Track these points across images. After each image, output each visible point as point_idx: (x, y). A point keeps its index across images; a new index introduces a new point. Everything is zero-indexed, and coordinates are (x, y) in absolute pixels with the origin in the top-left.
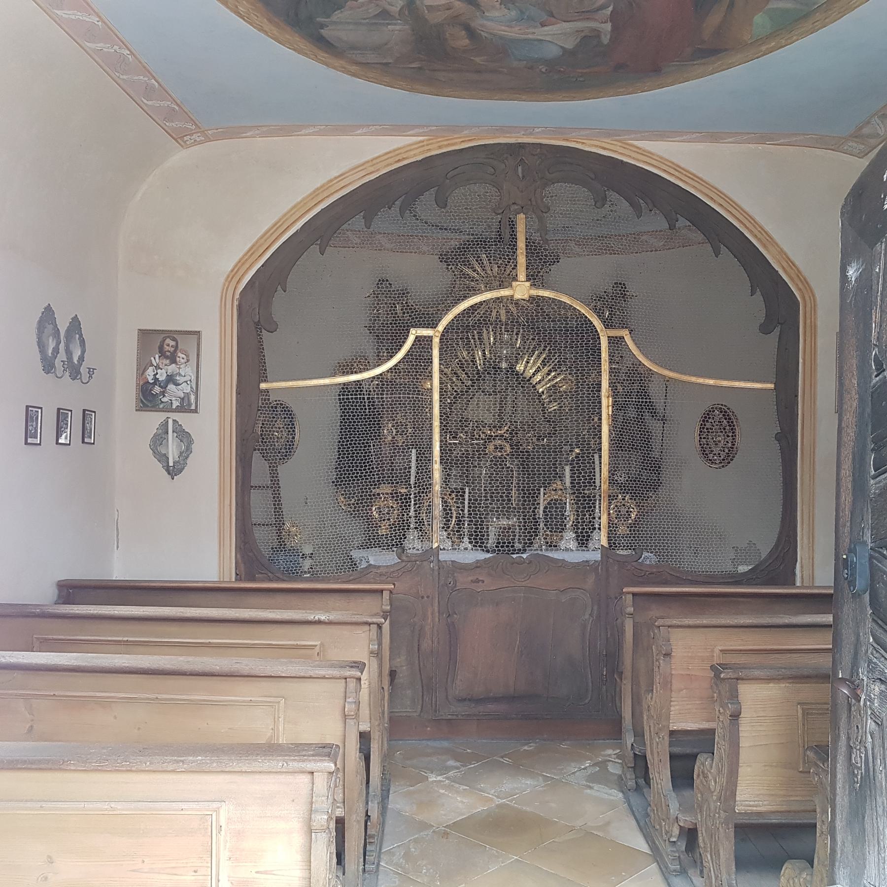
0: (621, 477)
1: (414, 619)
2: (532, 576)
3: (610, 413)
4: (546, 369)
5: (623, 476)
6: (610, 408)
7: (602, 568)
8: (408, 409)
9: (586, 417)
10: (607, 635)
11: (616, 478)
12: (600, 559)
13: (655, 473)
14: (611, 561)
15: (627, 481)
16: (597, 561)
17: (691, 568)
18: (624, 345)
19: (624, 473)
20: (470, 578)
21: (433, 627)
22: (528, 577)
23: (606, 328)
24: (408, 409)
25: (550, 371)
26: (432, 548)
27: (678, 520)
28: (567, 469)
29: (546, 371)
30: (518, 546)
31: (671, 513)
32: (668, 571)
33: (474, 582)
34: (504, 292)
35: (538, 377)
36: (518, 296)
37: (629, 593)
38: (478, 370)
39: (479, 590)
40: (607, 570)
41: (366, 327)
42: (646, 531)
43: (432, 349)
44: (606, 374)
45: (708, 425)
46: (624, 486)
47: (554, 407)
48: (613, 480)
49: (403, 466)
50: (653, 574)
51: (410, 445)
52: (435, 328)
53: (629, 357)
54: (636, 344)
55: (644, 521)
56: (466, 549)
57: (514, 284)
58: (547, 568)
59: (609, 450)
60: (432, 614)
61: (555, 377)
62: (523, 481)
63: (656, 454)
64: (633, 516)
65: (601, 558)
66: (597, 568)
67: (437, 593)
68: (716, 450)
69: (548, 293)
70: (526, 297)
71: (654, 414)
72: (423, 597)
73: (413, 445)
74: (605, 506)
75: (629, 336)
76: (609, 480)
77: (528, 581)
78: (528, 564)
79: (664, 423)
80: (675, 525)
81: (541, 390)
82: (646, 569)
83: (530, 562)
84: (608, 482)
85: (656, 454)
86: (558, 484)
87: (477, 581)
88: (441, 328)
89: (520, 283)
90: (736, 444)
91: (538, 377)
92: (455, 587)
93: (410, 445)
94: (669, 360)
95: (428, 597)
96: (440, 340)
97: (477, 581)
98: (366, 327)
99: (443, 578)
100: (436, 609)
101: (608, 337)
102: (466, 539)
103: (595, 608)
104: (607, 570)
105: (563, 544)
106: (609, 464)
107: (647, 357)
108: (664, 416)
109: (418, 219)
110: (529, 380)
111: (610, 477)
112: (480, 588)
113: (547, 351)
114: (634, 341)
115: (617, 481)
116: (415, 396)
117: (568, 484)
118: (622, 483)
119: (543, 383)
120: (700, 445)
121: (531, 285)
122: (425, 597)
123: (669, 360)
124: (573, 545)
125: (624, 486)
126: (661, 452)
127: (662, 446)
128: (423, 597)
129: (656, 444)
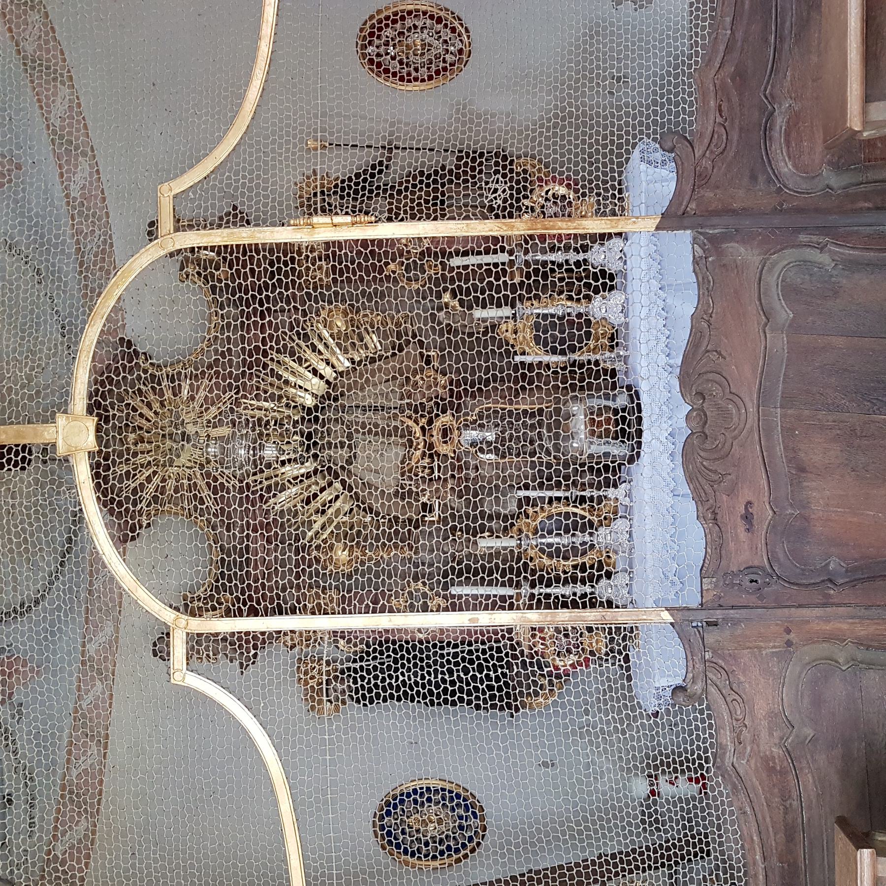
0: (496, 191)
1: (841, 660)
2: (733, 391)
3: (348, 219)
4: (309, 354)
5: (493, 186)
6: (337, 219)
7: (713, 227)
8: (355, 682)
9: (361, 276)
10: (869, 209)
11: (500, 202)
12: (688, 232)
13: (481, 164)
14: (693, 205)
15: (504, 176)
16: (694, 239)
17: (704, 20)
18: (194, 193)
19: (487, 183)
20: (743, 535)
21: (859, 617)
22: (736, 399)
23: (156, 238)
24: (355, 682)
25: (314, 348)
26: (672, 624)
27: (591, 54)
28: (479, 313)
29: (313, 355)
30: (622, 400)
31: (577, 73)
32: (713, 72)
33: (751, 524)
34: (83, 472)
35: (328, 372)
36: (90, 441)
37: (864, 112)
38: (316, 471)
39: (771, 512)
40: (716, 213)
41: (242, 672)
42: (620, 129)
43: (217, 634)
44: (261, 232)
45: (395, 66)
46: (518, 182)
47: (373, 341)
48: (505, 208)
49: (484, 693)
50: (720, 106)
51: (436, 677)
52: (168, 627)
53: (221, 182)
54: (191, 166)
55: (598, 133)
56: (628, 495)
57: (61, 451)
58: (714, 356)
59: (435, 219)
60: (827, 620)
61: (321, 338)
62: (495, 381)
63: (450, 162)
64: (562, 190)
65: (685, 228)
66: (712, 239)
67: (779, 612)
68: (438, 47)
69: (81, 370)
70: (91, 423)
71: (378, 168)
72: (789, 643)
73: (436, 671)
74: (564, 225)
75: (172, 184)
76: (504, 217)
77: (747, 400)
78: (704, 399)
79: (397, 148)
80: (605, 61)
81: (347, 364)
82: (711, 122)
83: (701, 395)
84: (508, 220)
85: (450, 162)
86: (506, 331)
87: (748, 518)
88: (168, 615)
89: (60, 437)
90: (424, 8)
91: (328, 372)
92: (763, 569)
93: (436, 677)
94: (226, 90)
95: (788, 631)
96: (195, 616)
97: (748, 518)
98: (242, 672)
99: (744, 599)
100: (818, 612)
101: (177, 230)
102: (611, 492)
103: (803, 238)
104: (716, 213)
105: (616, 319)
106: (467, 218)
107: (220, 139)
108: (384, 147)
109: (43, 596)
110: (328, 382)
111: (497, 216)
112: (764, 513)
113: (281, 357)
114: (183, 172)
115: (505, 200)
116: (324, 669)
117: (507, 311)
118: (511, 188)
119: (334, 360)
120: (430, 78)
121: (65, 412)
122: (788, 637)
123: (226, 90)
124: (616, 298)
125: (518, 182)
126: (446, 151)
127: (431, 150)
128: (789, 643)
129: (428, 162)
